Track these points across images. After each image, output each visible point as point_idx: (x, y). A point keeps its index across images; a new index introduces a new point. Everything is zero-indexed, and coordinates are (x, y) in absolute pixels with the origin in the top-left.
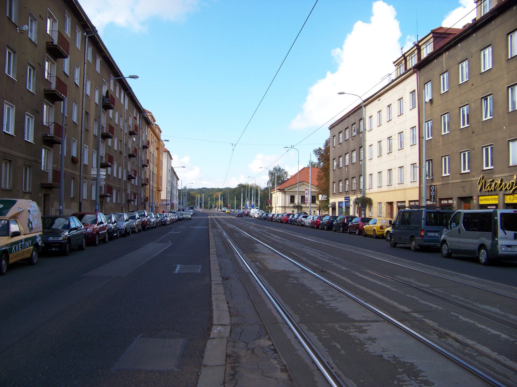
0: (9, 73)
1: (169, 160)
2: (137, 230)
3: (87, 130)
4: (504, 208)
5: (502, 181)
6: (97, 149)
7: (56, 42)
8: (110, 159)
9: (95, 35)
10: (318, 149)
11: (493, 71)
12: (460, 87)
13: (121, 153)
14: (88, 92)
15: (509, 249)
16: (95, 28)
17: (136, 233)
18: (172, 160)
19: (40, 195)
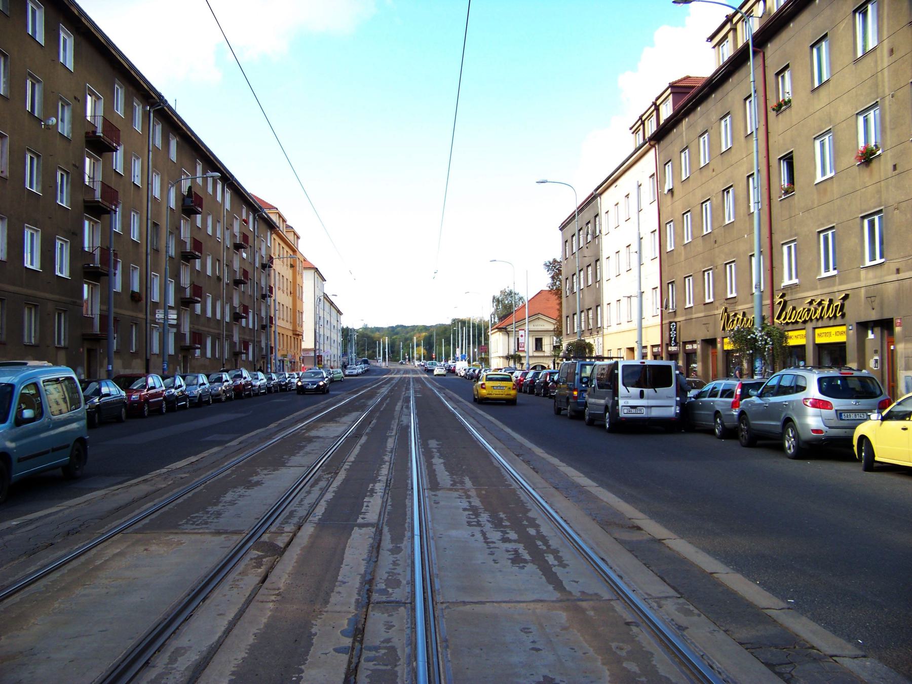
0: (31, 186)
1: (319, 282)
2: (223, 399)
3: (157, 251)
4: (667, 360)
5: (744, 315)
6: (176, 276)
7: (99, 133)
8: (197, 290)
9: (165, 108)
10: (551, 261)
11: (733, 151)
12: (701, 172)
13: (219, 279)
14: (157, 193)
15: (633, 411)
16: (163, 97)
17: (223, 402)
18: (324, 282)
19: (81, 350)
